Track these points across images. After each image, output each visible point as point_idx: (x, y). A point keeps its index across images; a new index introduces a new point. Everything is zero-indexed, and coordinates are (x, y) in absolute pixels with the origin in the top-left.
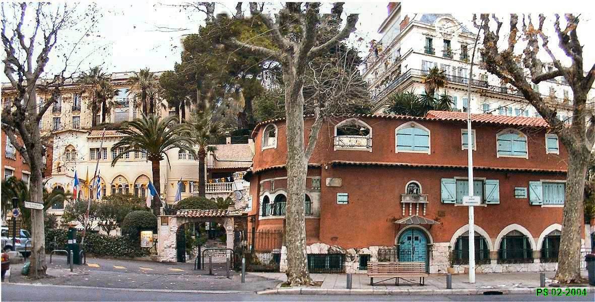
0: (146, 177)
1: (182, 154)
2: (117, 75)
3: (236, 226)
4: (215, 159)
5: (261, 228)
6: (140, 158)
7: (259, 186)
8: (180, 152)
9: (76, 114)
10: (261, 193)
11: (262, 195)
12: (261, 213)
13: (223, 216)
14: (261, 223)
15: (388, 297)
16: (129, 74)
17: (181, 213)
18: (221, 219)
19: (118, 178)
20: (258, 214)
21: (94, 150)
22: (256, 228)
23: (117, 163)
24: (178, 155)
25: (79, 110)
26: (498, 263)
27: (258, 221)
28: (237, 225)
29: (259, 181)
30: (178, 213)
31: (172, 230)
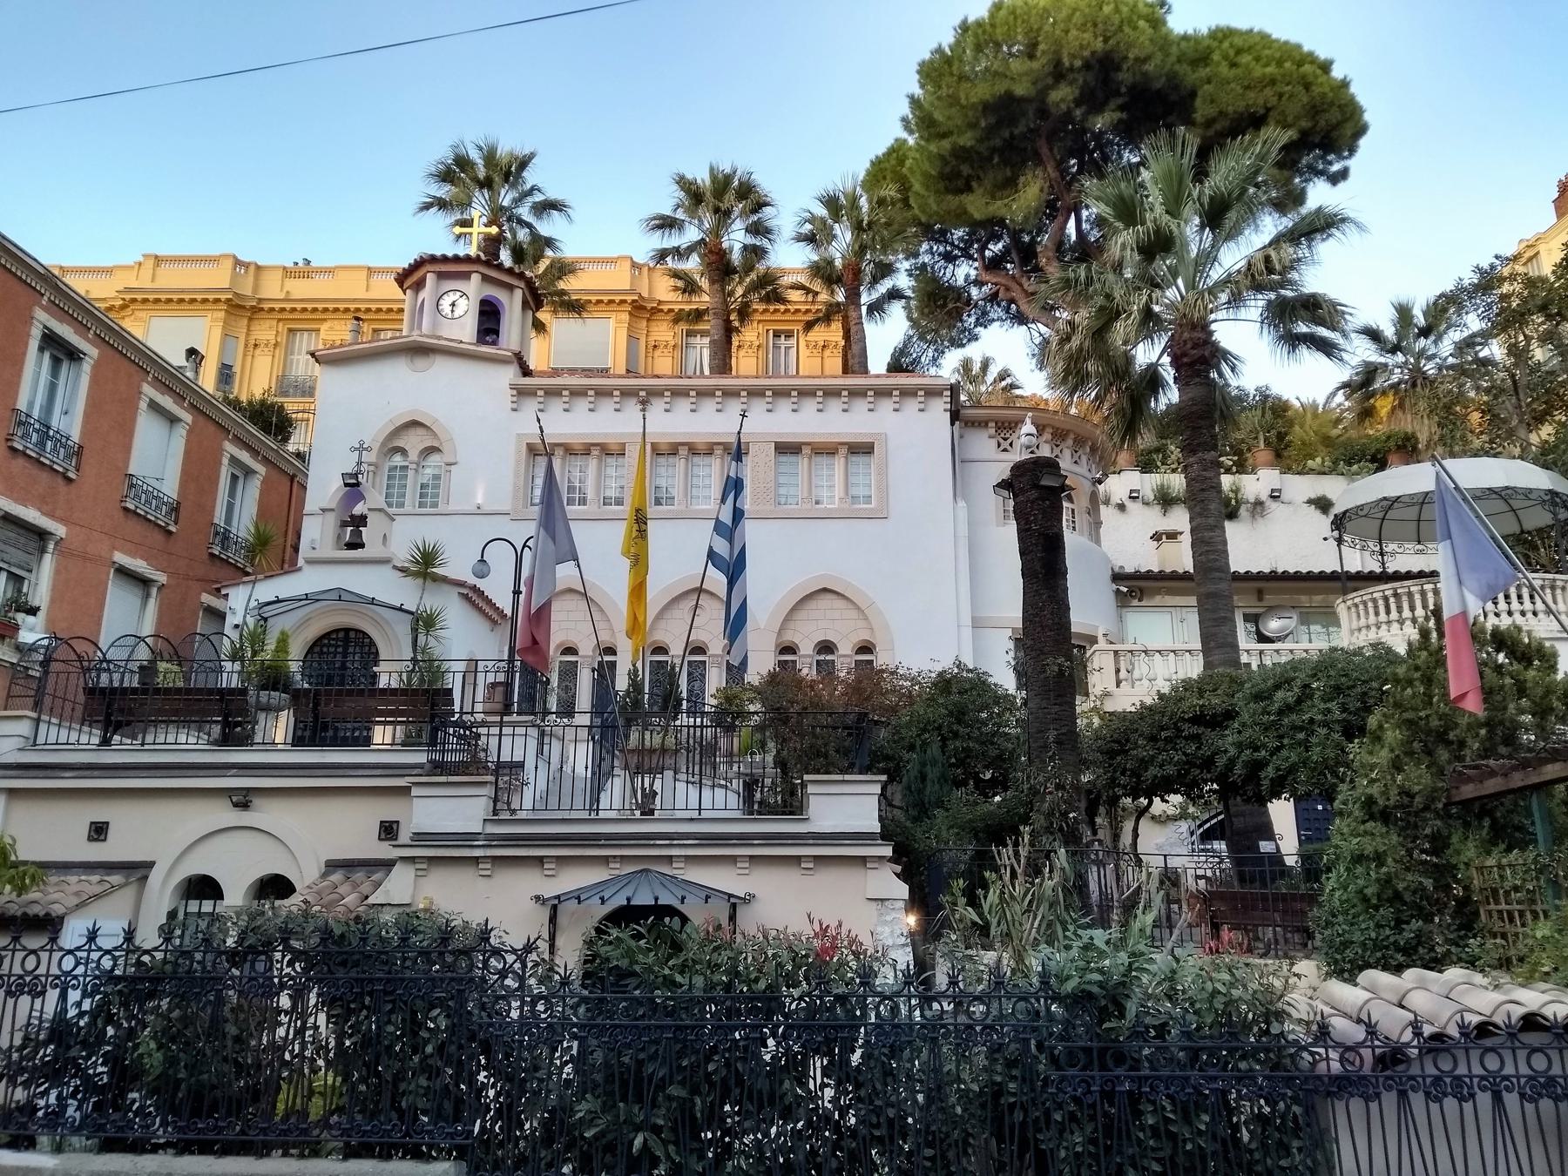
0: (840, 603)
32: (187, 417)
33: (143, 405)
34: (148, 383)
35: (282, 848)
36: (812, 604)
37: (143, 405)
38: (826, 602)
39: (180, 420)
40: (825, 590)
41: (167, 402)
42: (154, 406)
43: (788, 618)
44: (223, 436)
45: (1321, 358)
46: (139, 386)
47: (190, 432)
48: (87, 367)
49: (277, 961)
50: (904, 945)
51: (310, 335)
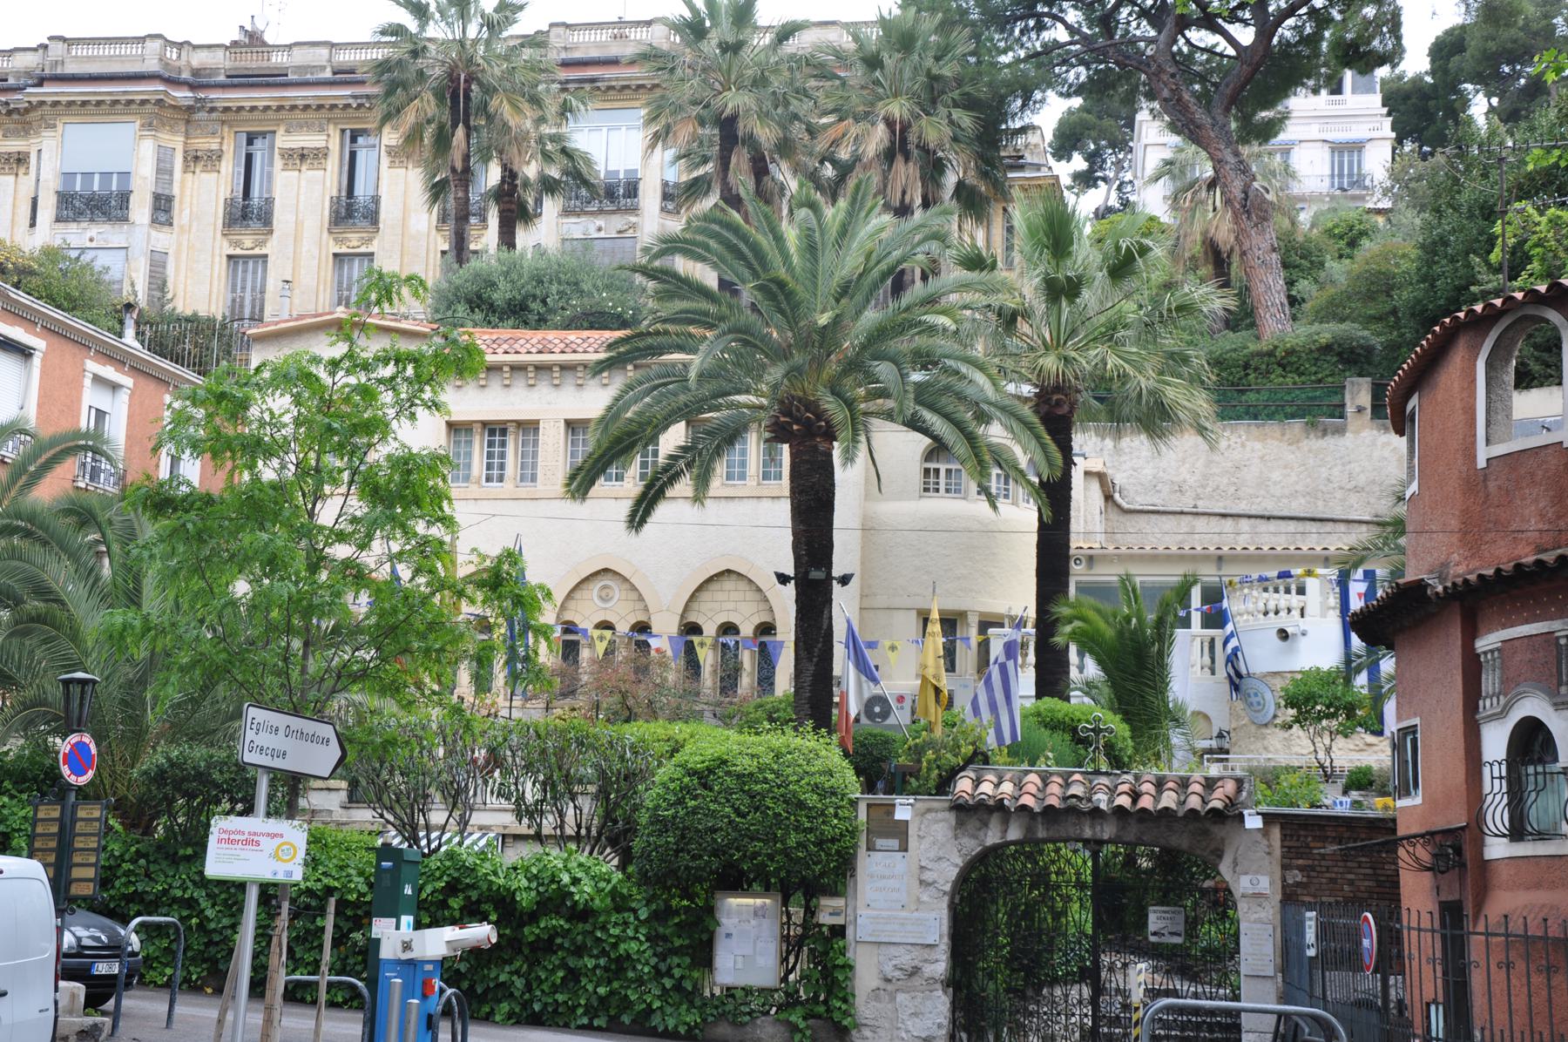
0: (742, 585)
1: (943, 467)
2: (577, 37)
3: (1296, 876)
4: (1108, 498)
5: (1506, 903)
6: (751, 482)
7: (1472, 667)
8: (930, 455)
9: (247, 242)
10: (1487, 706)
11: (1493, 718)
12: (1497, 814)
13: (1213, 810)
14: (1504, 874)
15: (326, 792)
16: (635, 34)
17: (977, 783)
18: (1206, 833)
19: (596, 587)
20: (1476, 828)
21: (504, 432)
22: (1469, 910)
23: (662, 511)
24: (408, 444)
25: (373, 217)
26: (489, 690)
27: (1484, 866)
28: (1301, 869)
29: (1470, 634)
30: (964, 785)
31: (928, 876)
32: (127, 381)
33: (88, 382)
34: (91, 358)
35: (1375, 142)
36: (714, 586)
37: (88, 382)
38: (729, 584)
39: (121, 386)
40: (729, 571)
41: (109, 372)
42: (97, 379)
43: (693, 597)
44: (164, 389)
45: (986, 504)
46: (83, 364)
47: (131, 397)
48: (37, 360)
49: (1086, 1015)
50: (957, 865)
51: (256, 263)
